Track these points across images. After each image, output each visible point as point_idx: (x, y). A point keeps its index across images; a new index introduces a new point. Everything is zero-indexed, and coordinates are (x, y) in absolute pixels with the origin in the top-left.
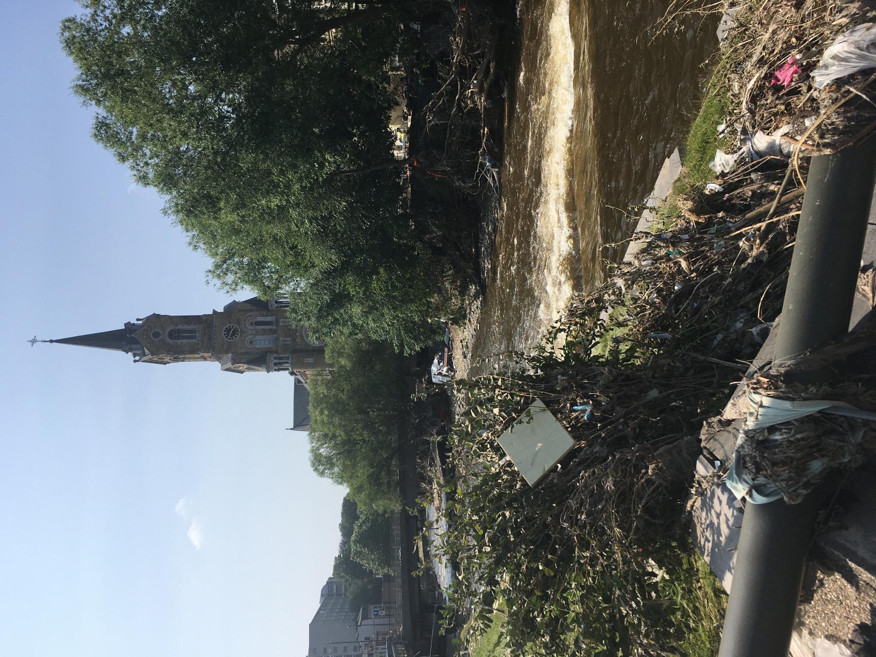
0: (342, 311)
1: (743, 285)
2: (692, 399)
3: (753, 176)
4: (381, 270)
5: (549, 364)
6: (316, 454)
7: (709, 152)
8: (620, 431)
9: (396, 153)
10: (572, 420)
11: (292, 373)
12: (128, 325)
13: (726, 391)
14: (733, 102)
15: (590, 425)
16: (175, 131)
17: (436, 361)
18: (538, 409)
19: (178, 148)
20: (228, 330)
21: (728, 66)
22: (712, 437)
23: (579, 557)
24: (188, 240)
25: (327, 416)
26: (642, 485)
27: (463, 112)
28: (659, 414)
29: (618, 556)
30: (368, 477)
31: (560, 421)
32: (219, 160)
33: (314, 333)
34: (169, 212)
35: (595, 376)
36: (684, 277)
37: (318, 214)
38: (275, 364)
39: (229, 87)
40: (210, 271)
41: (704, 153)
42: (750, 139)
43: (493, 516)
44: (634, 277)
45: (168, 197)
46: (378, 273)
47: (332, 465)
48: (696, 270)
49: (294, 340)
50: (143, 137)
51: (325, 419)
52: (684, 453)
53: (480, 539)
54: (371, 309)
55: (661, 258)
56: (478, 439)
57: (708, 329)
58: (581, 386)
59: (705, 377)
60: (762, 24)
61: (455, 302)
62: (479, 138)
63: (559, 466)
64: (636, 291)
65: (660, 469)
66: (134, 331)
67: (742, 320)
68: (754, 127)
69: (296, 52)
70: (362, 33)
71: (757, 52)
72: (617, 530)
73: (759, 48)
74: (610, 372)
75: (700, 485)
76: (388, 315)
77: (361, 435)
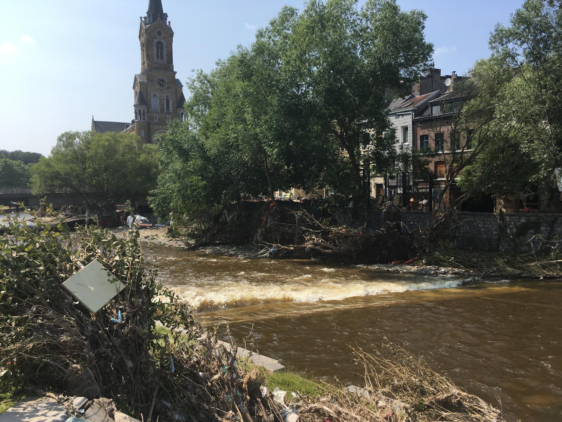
0: (177, 156)
1: (204, 416)
2: (127, 390)
3: (272, 415)
4: (204, 182)
5: (150, 293)
6: (75, 135)
7: (283, 387)
8: (103, 343)
9: (278, 192)
10: (110, 310)
11: (133, 122)
12: (166, 15)
13: (133, 413)
14: (314, 398)
15: (107, 322)
16: (290, 57)
17: (143, 218)
18: (118, 286)
19: (280, 58)
20: (163, 81)
21: (335, 393)
22: (101, 405)
23: (12, 319)
24: (222, 60)
25: (104, 144)
26: (64, 361)
27: (302, 234)
28: (115, 369)
29: (12, 347)
30: (57, 171)
31: (110, 302)
32: (273, 83)
33: (162, 137)
34: (240, 50)
35: (142, 324)
36: (208, 378)
37: (240, 142)
38: (140, 111)
39: (317, 93)
40: (202, 72)
41: (282, 384)
42: (293, 411)
43: (40, 258)
44: (208, 346)
45: (250, 49)
46: (202, 180)
47: (66, 147)
48: (212, 385)
49: (156, 124)
50: (286, 37)
51: (102, 143)
52: (87, 389)
53: (22, 249)
54: (179, 176)
55: (220, 361)
56: (96, 247)
57: (174, 397)
58: (135, 315)
59: (141, 398)
60: (360, 411)
61: (183, 231)
62: (287, 244)
63: (77, 303)
64: (199, 347)
65: (77, 372)
66: (162, 19)
67: (180, 419)
68: (301, 413)
69: (336, 133)
70: (347, 173)
71: (344, 410)
72: (31, 345)
73: (346, 411)
74: (145, 334)
75: (66, 401)
76: (176, 186)
77: (89, 167)
